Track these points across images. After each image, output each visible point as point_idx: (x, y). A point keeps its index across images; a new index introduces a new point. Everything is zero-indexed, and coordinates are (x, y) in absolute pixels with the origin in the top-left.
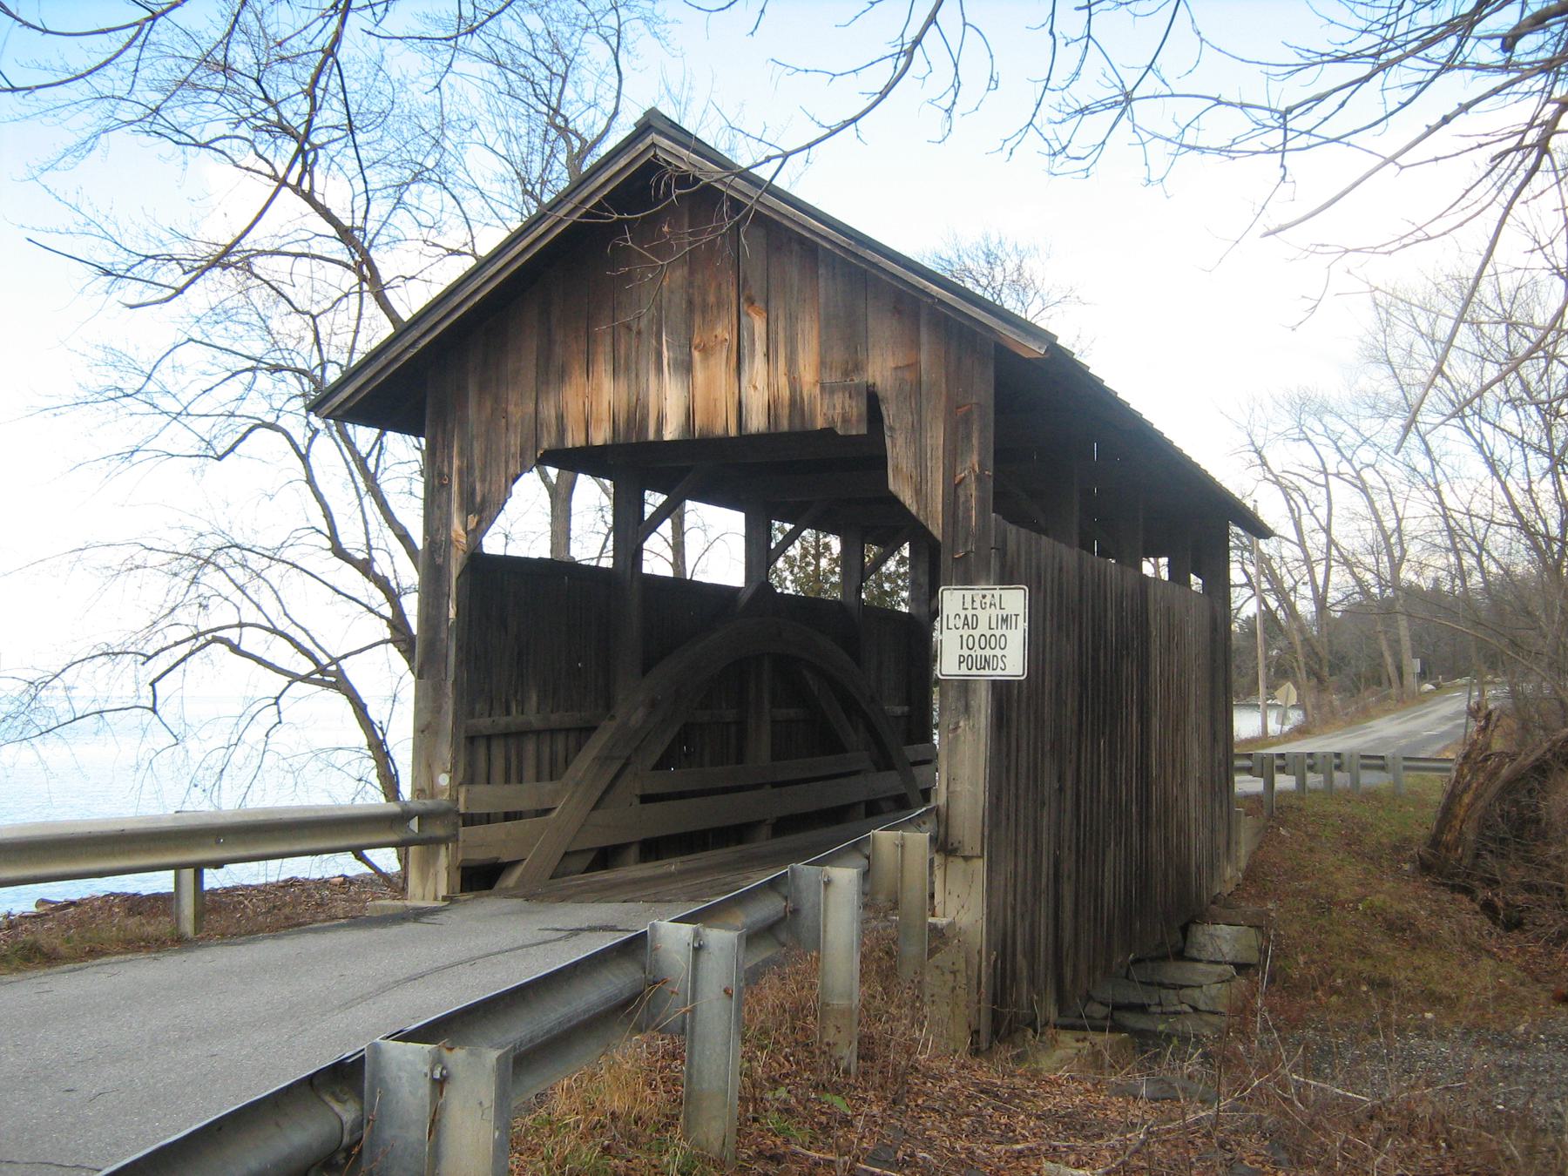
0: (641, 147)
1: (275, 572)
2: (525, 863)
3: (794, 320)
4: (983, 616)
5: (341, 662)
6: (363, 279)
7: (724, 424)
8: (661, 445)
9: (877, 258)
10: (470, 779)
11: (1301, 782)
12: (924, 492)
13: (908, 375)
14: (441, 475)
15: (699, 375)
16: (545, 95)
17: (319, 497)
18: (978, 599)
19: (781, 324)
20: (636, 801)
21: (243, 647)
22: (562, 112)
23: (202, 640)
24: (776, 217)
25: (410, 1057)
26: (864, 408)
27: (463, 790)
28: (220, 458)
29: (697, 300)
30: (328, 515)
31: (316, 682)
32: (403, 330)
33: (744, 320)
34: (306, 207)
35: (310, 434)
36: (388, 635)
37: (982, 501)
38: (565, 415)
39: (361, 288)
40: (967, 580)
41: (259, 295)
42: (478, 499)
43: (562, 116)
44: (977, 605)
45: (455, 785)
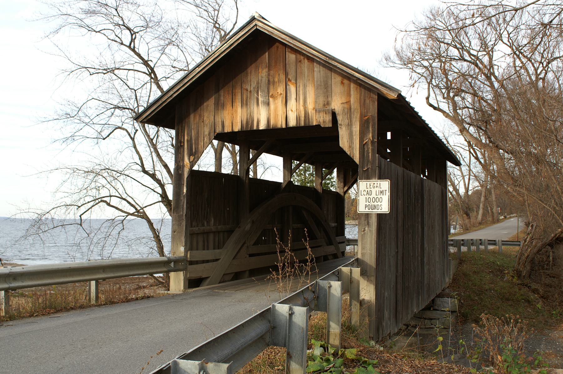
0: (252, 26)
1: (121, 178)
2: (210, 278)
3: (305, 86)
4: (374, 191)
5: (144, 209)
6: (152, 78)
7: (281, 123)
8: (258, 131)
9: (336, 64)
10: (191, 249)
11: (469, 249)
12: (352, 147)
13: (346, 106)
14: (181, 142)
15: (272, 106)
16: (212, 16)
17: (138, 153)
18: (372, 185)
19: (301, 88)
20: (248, 256)
21: (111, 204)
22: (218, 22)
23: (97, 201)
24: (300, 50)
25: (189, 366)
26: (331, 118)
27: (189, 252)
28: (104, 139)
29: (271, 80)
30: (141, 159)
31: (135, 216)
32: (164, 94)
33: (288, 87)
34: (132, 53)
35: (135, 131)
36: (160, 199)
37: (373, 150)
38: (224, 121)
39: (151, 81)
40: (368, 178)
41: (117, 83)
42: (194, 150)
43: (218, 24)
44: (371, 187)
45: (186, 251)
